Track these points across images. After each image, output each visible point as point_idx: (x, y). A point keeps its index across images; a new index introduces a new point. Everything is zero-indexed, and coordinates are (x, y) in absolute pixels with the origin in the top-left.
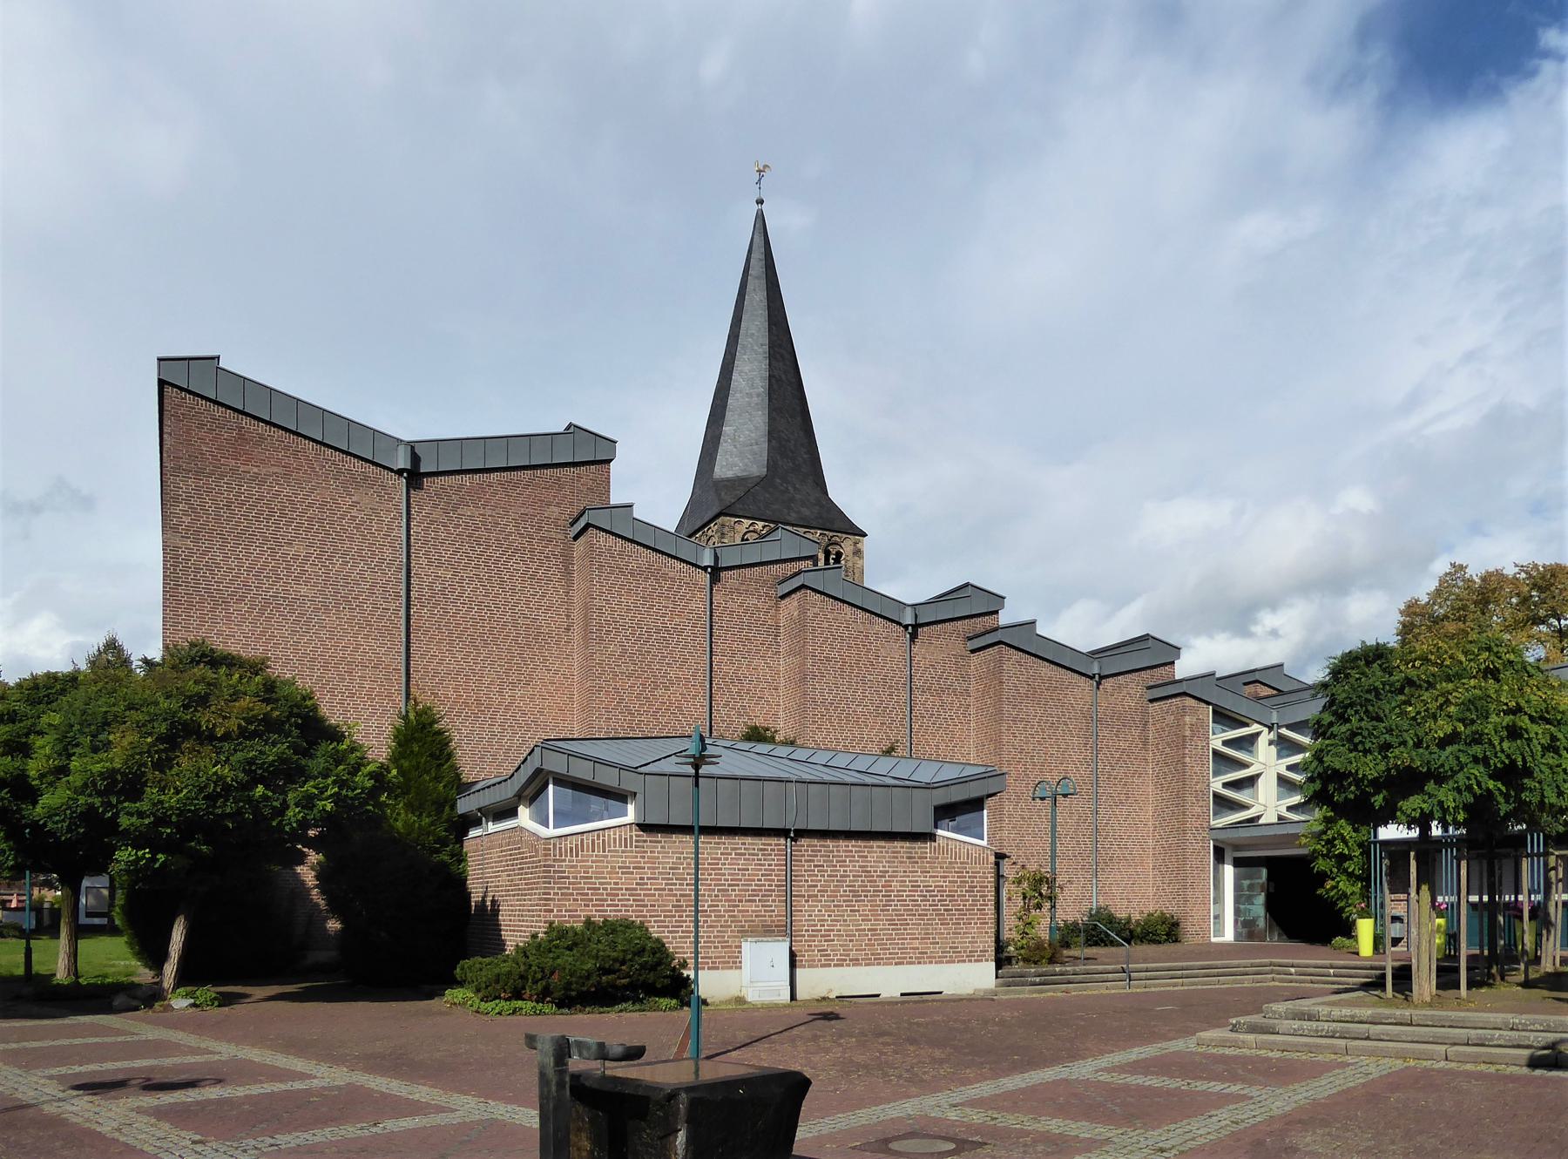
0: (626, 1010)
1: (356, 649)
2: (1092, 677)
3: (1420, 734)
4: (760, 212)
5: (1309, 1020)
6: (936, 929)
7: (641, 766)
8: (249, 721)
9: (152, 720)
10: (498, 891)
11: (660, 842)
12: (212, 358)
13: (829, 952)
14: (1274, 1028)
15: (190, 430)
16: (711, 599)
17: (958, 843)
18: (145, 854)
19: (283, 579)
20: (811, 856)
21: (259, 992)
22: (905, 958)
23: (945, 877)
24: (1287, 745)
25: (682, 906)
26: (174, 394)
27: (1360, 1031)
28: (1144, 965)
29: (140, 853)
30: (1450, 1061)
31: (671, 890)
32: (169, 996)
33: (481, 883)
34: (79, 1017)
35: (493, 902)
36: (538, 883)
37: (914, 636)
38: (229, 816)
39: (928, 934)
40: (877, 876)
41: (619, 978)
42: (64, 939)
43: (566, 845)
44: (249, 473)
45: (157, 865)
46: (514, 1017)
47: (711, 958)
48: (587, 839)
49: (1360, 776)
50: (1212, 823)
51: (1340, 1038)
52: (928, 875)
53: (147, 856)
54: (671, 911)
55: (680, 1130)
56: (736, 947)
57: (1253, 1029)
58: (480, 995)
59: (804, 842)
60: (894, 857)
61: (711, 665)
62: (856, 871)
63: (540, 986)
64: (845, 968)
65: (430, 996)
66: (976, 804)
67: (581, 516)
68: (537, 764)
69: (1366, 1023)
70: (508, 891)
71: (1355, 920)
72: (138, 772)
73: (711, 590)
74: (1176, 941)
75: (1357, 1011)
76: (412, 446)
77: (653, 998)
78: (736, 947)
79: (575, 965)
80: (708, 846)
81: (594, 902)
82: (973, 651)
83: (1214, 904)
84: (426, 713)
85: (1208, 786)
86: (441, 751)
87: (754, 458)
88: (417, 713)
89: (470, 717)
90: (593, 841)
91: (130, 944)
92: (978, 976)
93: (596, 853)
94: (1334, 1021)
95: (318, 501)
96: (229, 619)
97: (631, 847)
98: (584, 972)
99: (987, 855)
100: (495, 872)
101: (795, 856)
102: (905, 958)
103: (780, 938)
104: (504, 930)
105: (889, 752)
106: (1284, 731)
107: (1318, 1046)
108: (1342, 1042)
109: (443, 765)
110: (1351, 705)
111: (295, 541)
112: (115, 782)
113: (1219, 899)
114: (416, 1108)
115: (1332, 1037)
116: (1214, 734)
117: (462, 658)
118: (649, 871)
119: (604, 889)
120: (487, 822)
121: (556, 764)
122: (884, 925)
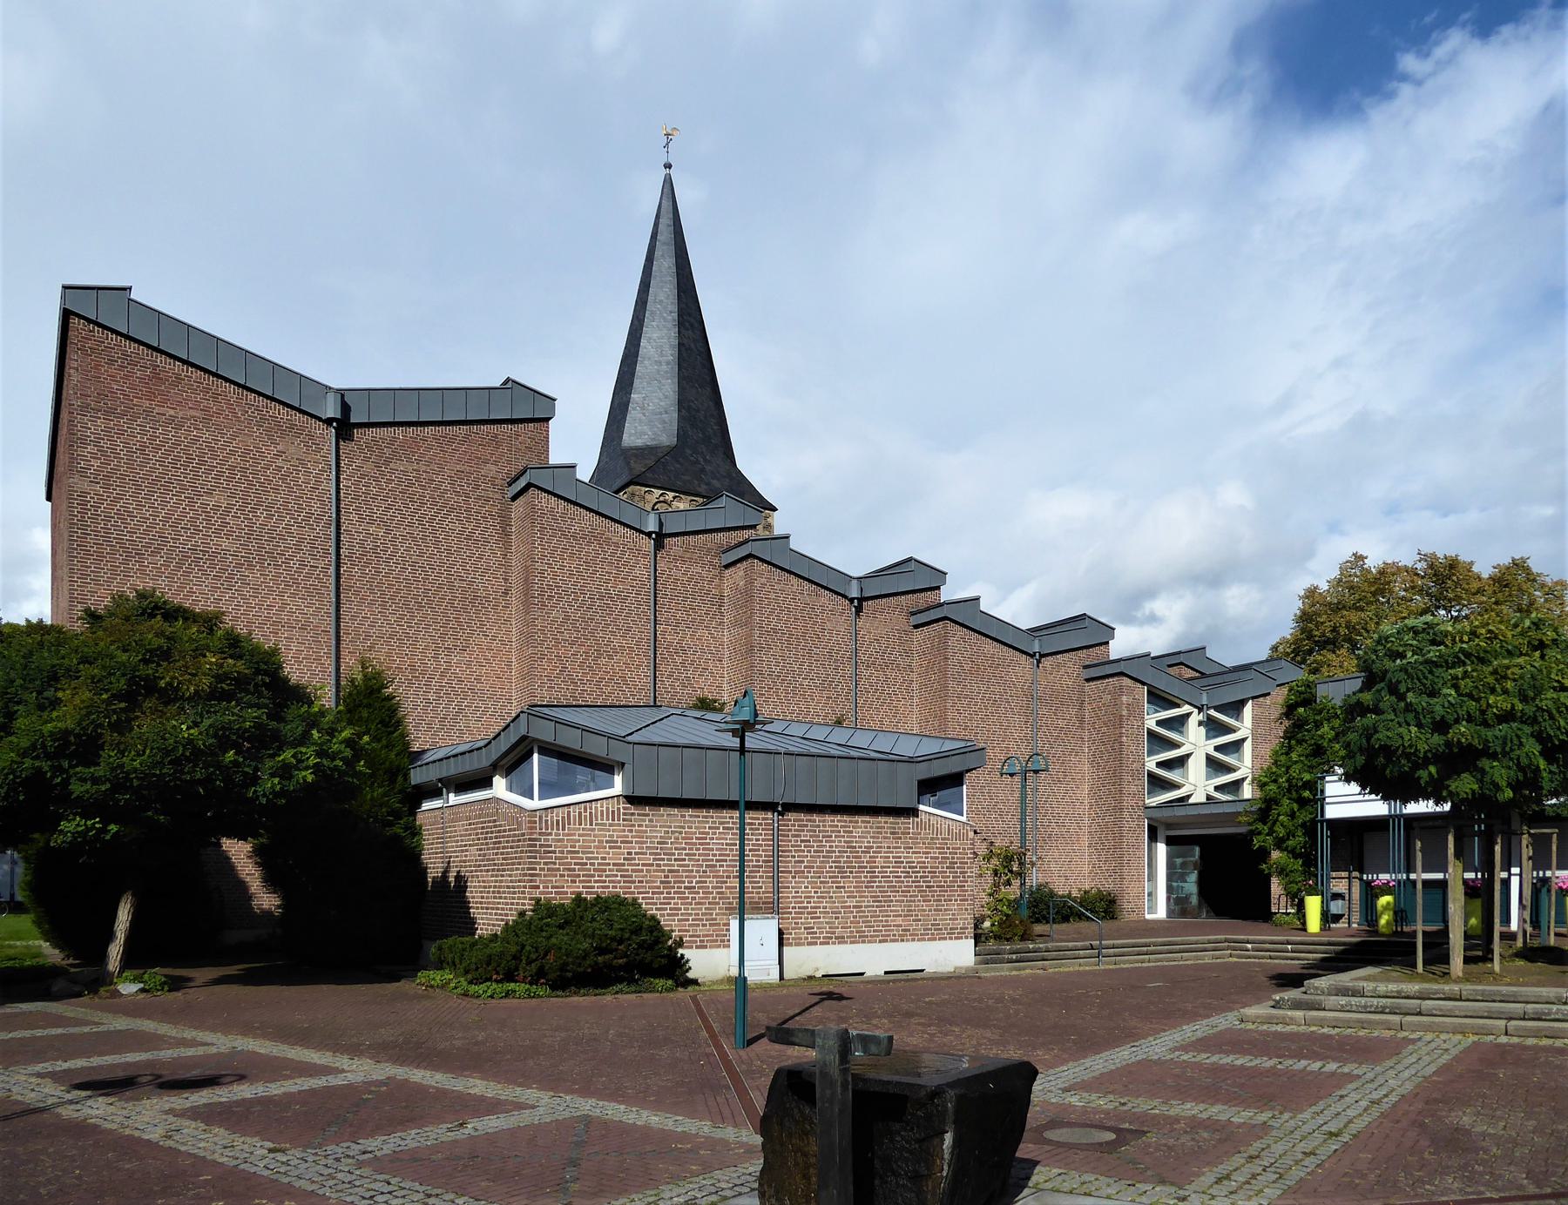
0: (621, 992)
1: (282, 609)
2: (1032, 656)
4: (668, 177)
5: (1353, 996)
6: (918, 906)
7: (627, 735)
8: (220, 678)
9: (110, 674)
10: (466, 867)
11: (648, 815)
12: (124, 289)
13: (815, 930)
14: (1320, 1004)
15: (100, 365)
16: (655, 566)
18: (94, 823)
19: (202, 531)
22: (889, 935)
23: (927, 853)
25: (670, 882)
27: (1412, 1006)
28: (1111, 942)
29: (89, 823)
30: (1510, 1035)
33: (442, 858)
34: (21, 1005)
35: (459, 877)
36: (521, 858)
37: (859, 610)
38: (200, 782)
39: (911, 911)
40: (862, 852)
41: (615, 958)
44: (165, 415)
45: (108, 837)
48: (574, 811)
50: (1147, 801)
51: (1390, 1013)
53: (97, 826)
54: (659, 888)
55: (947, 1132)
56: (724, 925)
57: (1297, 1005)
58: (469, 976)
59: (791, 816)
60: (878, 833)
61: (655, 634)
62: (841, 847)
64: (831, 947)
65: (394, 978)
66: (956, 780)
67: (522, 475)
68: (523, 732)
70: (480, 866)
71: (1304, 897)
72: (94, 734)
73: (656, 557)
74: (1112, 918)
75: (1404, 987)
76: (342, 393)
78: (724, 925)
79: (570, 945)
80: (696, 819)
81: (581, 878)
82: (916, 627)
85: (1144, 765)
86: (391, 717)
88: (365, 676)
89: (404, 683)
90: (580, 813)
91: (38, 923)
92: (957, 954)
93: (583, 826)
94: (1379, 997)
96: (143, 572)
97: (619, 820)
98: (580, 952)
100: (461, 846)
101: (782, 830)
102: (889, 935)
103: (769, 915)
104: (473, 908)
105: (839, 723)
106: (1212, 712)
107: (1370, 1022)
108: (1396, 1018)
109: (394, 733)
111: (215, 490)
112: (67, 744)
113: (1152, 877)
116: (1148, 714)
117: (395, 621)
119: (591, 864)
121: (545, 732)
122: (868, 901)
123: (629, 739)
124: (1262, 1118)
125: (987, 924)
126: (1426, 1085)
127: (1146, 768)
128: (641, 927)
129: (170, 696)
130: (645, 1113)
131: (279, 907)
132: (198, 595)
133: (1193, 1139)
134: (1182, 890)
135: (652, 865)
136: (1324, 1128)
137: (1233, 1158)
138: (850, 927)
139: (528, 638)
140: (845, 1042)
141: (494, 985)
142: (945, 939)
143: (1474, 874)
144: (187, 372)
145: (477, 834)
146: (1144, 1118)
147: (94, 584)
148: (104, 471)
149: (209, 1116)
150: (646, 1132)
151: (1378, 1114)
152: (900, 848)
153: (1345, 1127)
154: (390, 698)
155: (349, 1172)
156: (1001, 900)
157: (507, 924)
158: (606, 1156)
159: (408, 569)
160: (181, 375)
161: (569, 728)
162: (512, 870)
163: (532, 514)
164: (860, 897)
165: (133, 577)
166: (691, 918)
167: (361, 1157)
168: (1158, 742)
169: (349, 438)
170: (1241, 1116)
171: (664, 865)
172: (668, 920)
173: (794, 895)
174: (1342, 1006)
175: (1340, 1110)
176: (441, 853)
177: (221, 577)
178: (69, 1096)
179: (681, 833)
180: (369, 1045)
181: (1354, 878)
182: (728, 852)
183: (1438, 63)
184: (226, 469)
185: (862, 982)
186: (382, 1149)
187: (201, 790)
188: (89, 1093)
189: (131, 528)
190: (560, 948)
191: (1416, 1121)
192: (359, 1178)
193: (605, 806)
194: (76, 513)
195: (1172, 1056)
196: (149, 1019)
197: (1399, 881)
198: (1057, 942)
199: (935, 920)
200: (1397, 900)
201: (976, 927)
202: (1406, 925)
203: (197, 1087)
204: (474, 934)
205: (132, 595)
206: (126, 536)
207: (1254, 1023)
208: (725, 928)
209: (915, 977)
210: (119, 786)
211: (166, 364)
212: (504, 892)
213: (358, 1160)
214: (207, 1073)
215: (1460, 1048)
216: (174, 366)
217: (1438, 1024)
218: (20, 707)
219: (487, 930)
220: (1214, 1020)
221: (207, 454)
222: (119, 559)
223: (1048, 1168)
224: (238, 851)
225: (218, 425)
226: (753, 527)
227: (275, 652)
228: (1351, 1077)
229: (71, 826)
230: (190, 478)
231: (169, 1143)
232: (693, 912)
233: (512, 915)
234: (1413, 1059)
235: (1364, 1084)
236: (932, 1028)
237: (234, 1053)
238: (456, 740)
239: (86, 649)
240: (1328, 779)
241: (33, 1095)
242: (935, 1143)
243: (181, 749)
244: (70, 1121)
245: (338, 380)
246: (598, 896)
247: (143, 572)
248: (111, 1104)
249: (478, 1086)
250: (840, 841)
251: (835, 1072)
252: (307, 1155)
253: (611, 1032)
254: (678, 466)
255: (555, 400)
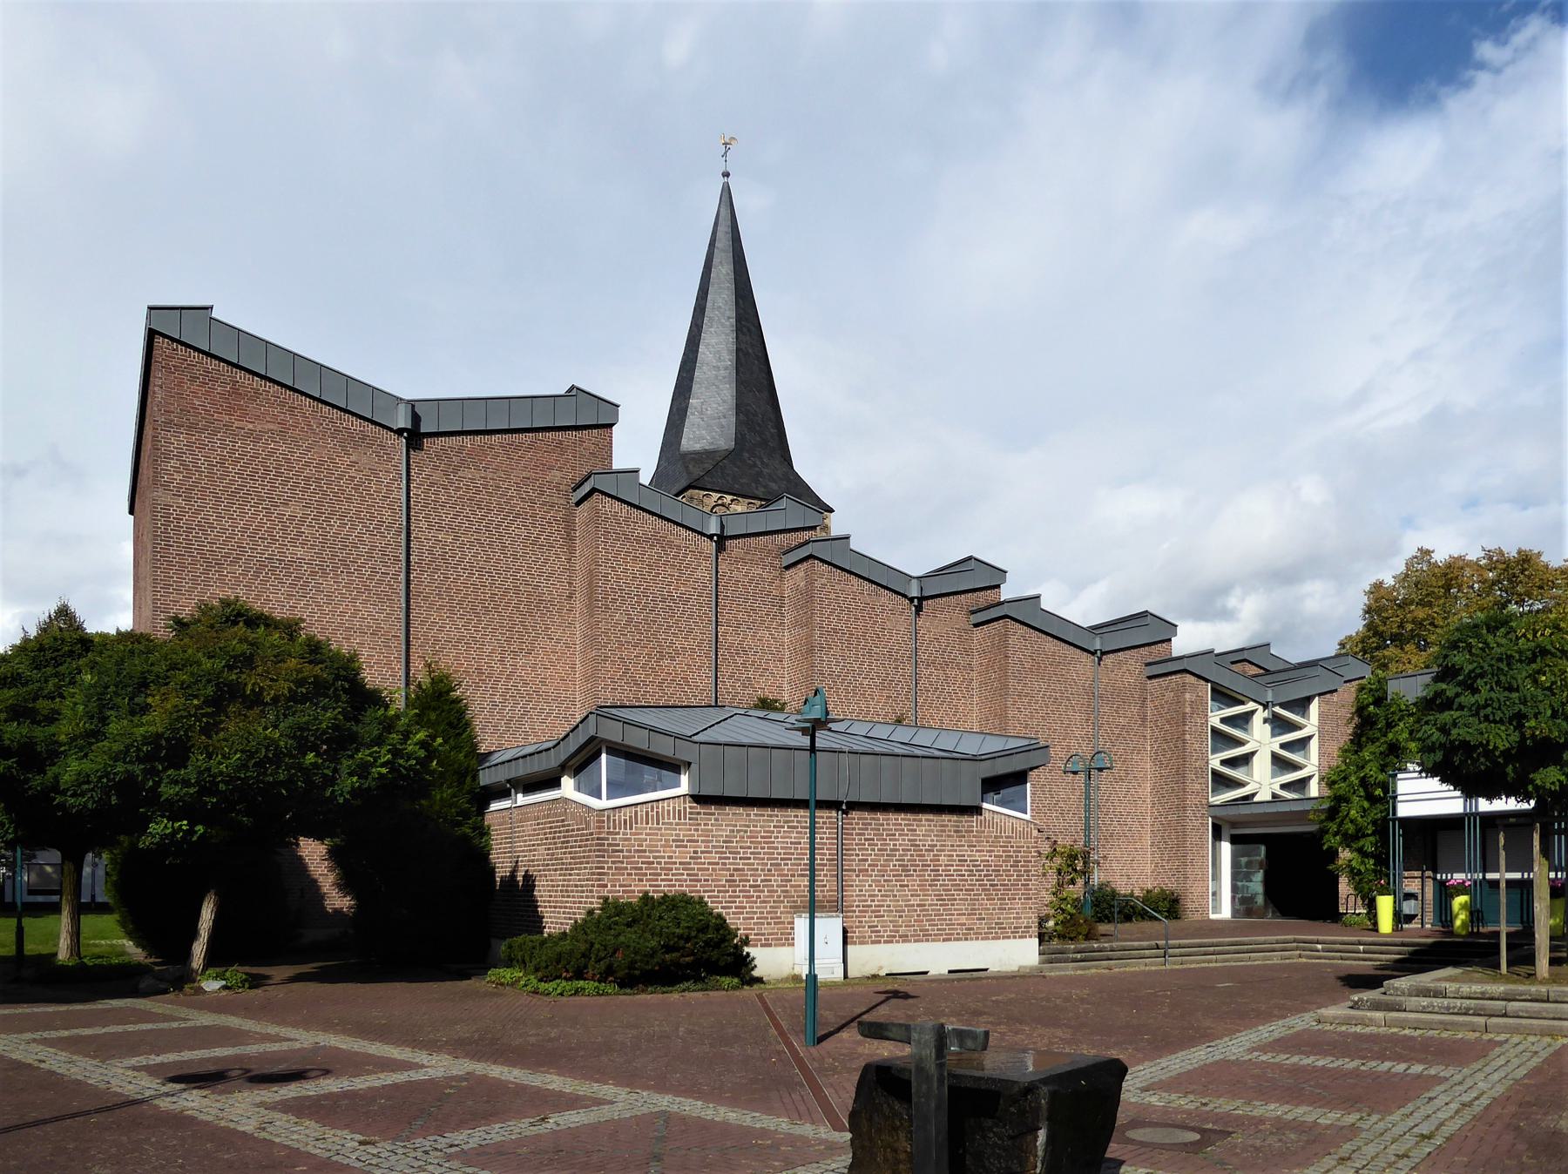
0: (688, 989)
1: (354, 615)
2: (1093, 653)
3: (1555, 705)
4: (726, 186)
5: (1434, 997)
7: (694, 735)
8: (300, 683)
10: (534, 866)
11: (714, 814)
13: (879, 928)
14: (1400, 1005)
15: (181, 382)
16: (717, 568)
17: (1003, 816)
18: (181, 825)
20: (862, 829)
21: (279, 972)
24: (1279, 723)
25: (735, 881)
26: (165, 345)
28: (1177, 942)
29: (177, 825)
31: (724, 864)
32: (199, 978)
35: (527, 877)
36: (589, 857)
37: (919, 609)
38: (281, 784)
39: (975, 909)
40: (926, 850)
41: (683, 956)
42: (65, 919)
43: (620, 817)
44: (244, 429)
45: (195, 838)
46: (576, 998)
47: (763, 934)
48: (641, 811)
49: (1491, 748)
50: (1211, 800)
51: (1473, 1015)
52: (975, 849)
53: (184, 828)
54: (725, 886)
55: (1041, 1129)
56: (789, 923)
57: (1377, 1006)
58: (540, 974)
59: (855, 814)
60: (942, 831)
61: (717, 635)
63: (603, 966)
65: (465, 976)
66: (1019, 778)
67: (586, 480)
68: (592, 732)
69: (1498, 999)
70: (548, 865)
73: (717, 559)
74: (1176, 918)
76: (412, 404)
77: (714, 977)
78: (789, 923)
79: (638, 943)
80: (762, 818)
81: (648, 877)
82: (976, 625)
83: (1213, 880)
84: (442, 681)
85: (1207, 763)
86: (459, 720)
87: (722, 431)
88: (432, 679)
89: (471, 686)
90: (647, 813)
91: (123, 924)
92: (1022, 953)
94: (1462, 998)
95: (315, 460)
96: (222, 581)
97: (685, 819)
99: (1031, 828)
100: (529, 846)
101: (847, 829)
103: (834, 914)
105: (899, 721)
106: (1277, 709)
107: (1453, 1024)
108: (1481, 1020)
109: (462, 734)
110: (1482, 676)
112: (158, 747)
113: (1216, 876)
114: (574, 1102)
115: (1465, 1014)
116: (1212, 712)
118: (703, 845)
120: (516, 794)
121: (612, 732)
123: (695, 738)
124: (1350, 1121)
125: (1051, 923)
126: (1518, 1087)
127: (1210, 766)
128: (708, 925)
129: (256, 700)
130: (722, 1110)
131: (350, 907)
132: (275, 602)
133: (1280, 1140)
134: (1247, 890)
135: (718, 864)
136: (1415, 1130)
137: (1324, 1160)
138: (914, 926)
139: (592, 641)
140: (941, 1037)
141: (564, 983)
142: (1009, 937)
143: (1520, 874)
144: (265, 387)
145: (545, 834)
146: (1226, 1118)
147: (177, 594)
148: (186, 485)
149: (299, 1108)
150: (725, 1129)
151: (1471, 1117)
152: (964, 846)
153: (1437, 1129)
154: (458, 701)
155: (438, 1164)
156: (1065, 899)
157: (576, 922)
158: (688, 1152)
159: (475, 574)
160: (259, 390)
161: (635, 727)
162: (580, 869)
163: (596, 517)
164: (924, 895)
165: (213, 586)
166: (755, 916)
167: (450, 1151)
168: (1221, 739)
169: (419, 447)
170: (1328, 1117)
171: (730, 864)
172: (734, 918)
173: (858, 893)
174: (1424, 1007)
175: (1430, 1112)
176: (509, 852)
177: (296, 585)
178: (164, 1089)
179: (746, 832)
180: (446, 1042)
181: (1427, 877)
182: (792, 851)
183: (1516, 50)
184: (302, 480)
185: (926, 981)
186: (468, 1142)
187: (284, 792)
188: (183, 1086)
189: (211, 539)
190: (629, 946)
191: (1509, 1125)
192: (448, 1170)
193: (671, 805)
194: (159, 525)
195: (1250, 1057)
196: (234, 1015)
197: (1475, 882)
198: (1121, 941)
199: (999, 918)
200: (1474, 900)
201: (1040, 925)
202: (1483, 927)
203: (285, 1081)
204: (542, 933)
205: (215, 603)
206: (206, 546)
207: (1331, 1024)
208: (789, 926)
209: (979, 976)
210: (207, 788)
211: (244, 379)
212: (572, 891)
213: (446, 1153)
214: (294, 1067)
215: (1551, 1050)
216: (253, 381)
217: (1525, 1027)
218: (112, 712)
219: (555, 928)
220: (1291, 1021)
221: (284, 465)
222: (200, 569)
223: (1134, 1168)
224: (313, 852)
225: (293, 437)
226: (813, 528)
227: (353, 658)
228: (1438, 1080)
229: (159, 827)
230: (268, 490)
231: (263, 1135)
232: (758, 910)
233: (580, 914)
234: (1502, 1061)
235: (1452, 1087)
236: (1002, 1027)
237: (317, 1048)
238: (521, 742)
239: (174, 656)
240: (1399, 776)
241: (131, 1087)
242: (1028, 1140)
243: (264, 750)
244: (167, 1112)
245: (409, 390)
246: (666, 895)
247: (222, 581)
248: (205, 1097)
249: (554, 1082)
250: (904, 840)
251: (932, 1067)
252: (396, 1147)
253: (681, 1029)
254: (736, 469)
255: (618, 406)
